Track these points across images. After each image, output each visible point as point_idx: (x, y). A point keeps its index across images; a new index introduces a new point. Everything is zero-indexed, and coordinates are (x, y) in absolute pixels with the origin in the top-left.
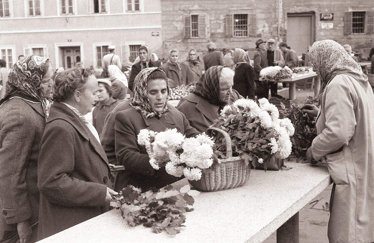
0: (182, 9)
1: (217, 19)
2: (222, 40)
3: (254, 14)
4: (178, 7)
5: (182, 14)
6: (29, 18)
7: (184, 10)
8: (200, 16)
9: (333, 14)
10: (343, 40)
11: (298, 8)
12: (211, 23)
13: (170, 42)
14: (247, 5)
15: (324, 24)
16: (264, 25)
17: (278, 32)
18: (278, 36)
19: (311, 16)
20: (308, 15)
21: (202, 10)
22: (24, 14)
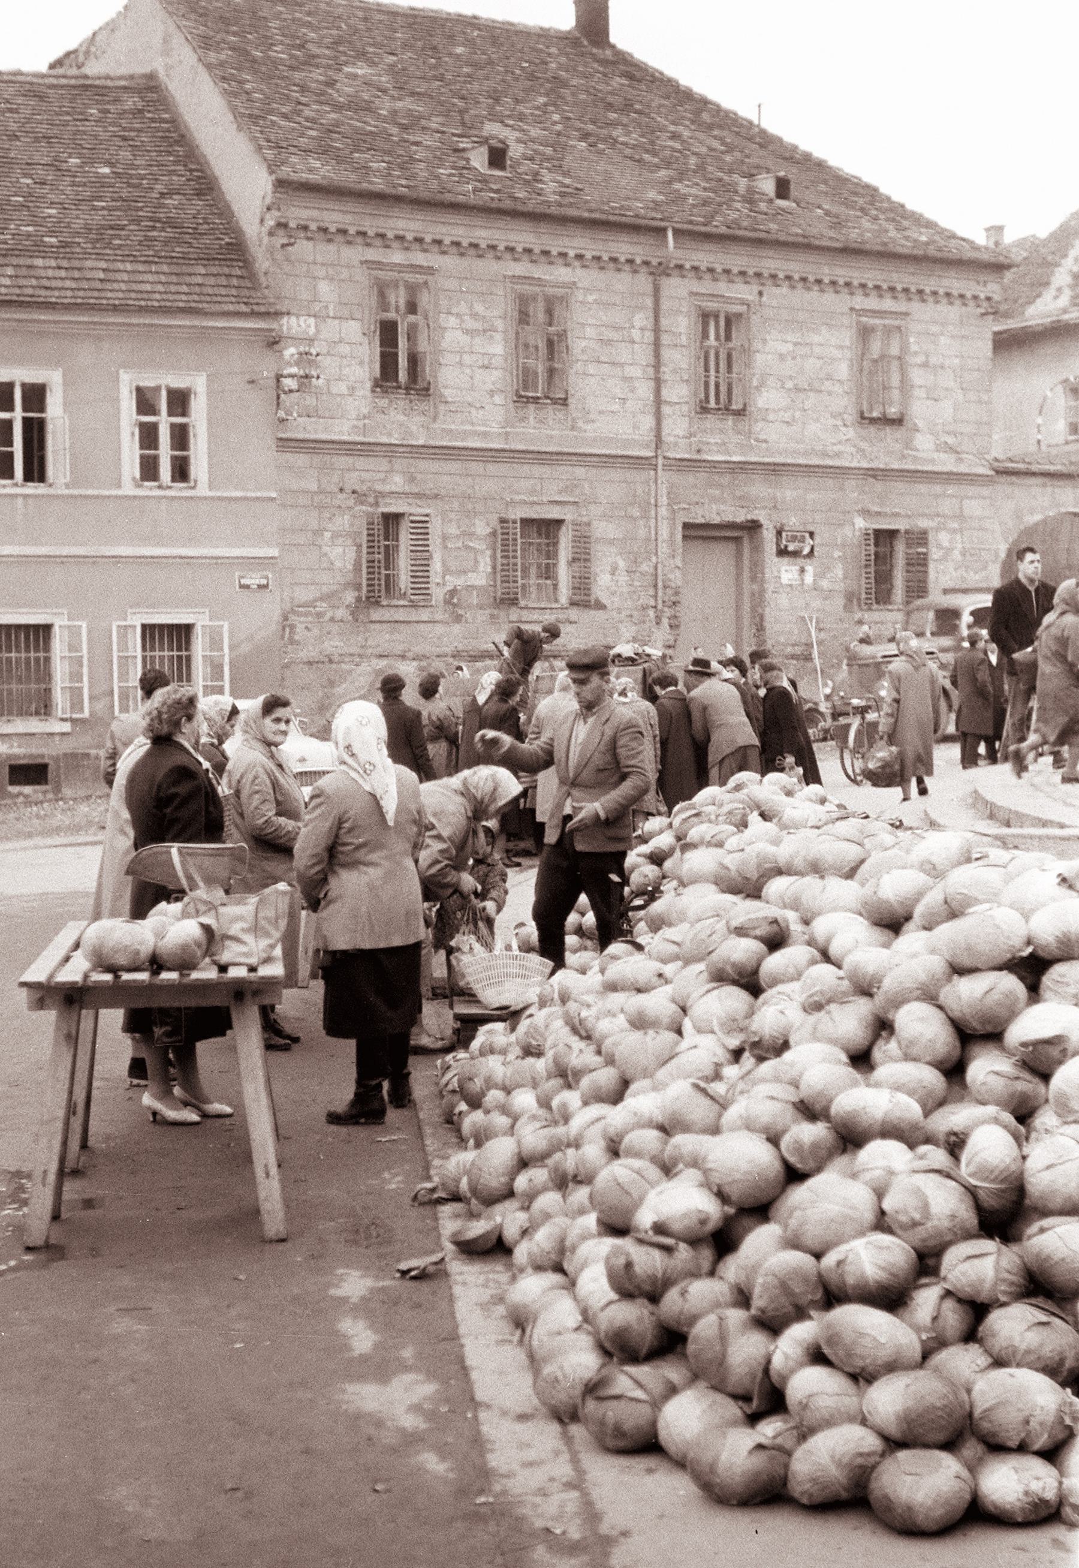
0: (348, 488)
1: (464, 534)
2: (482, 616)
3: (585, 519)
5: (350, 508)
7: (354, 492)
8: (412, 518)
9: (812, 534)
12: (446, 547)
13: (306, 615)
19: (737, 540)
20: (729, 534)
21: (419, 496)
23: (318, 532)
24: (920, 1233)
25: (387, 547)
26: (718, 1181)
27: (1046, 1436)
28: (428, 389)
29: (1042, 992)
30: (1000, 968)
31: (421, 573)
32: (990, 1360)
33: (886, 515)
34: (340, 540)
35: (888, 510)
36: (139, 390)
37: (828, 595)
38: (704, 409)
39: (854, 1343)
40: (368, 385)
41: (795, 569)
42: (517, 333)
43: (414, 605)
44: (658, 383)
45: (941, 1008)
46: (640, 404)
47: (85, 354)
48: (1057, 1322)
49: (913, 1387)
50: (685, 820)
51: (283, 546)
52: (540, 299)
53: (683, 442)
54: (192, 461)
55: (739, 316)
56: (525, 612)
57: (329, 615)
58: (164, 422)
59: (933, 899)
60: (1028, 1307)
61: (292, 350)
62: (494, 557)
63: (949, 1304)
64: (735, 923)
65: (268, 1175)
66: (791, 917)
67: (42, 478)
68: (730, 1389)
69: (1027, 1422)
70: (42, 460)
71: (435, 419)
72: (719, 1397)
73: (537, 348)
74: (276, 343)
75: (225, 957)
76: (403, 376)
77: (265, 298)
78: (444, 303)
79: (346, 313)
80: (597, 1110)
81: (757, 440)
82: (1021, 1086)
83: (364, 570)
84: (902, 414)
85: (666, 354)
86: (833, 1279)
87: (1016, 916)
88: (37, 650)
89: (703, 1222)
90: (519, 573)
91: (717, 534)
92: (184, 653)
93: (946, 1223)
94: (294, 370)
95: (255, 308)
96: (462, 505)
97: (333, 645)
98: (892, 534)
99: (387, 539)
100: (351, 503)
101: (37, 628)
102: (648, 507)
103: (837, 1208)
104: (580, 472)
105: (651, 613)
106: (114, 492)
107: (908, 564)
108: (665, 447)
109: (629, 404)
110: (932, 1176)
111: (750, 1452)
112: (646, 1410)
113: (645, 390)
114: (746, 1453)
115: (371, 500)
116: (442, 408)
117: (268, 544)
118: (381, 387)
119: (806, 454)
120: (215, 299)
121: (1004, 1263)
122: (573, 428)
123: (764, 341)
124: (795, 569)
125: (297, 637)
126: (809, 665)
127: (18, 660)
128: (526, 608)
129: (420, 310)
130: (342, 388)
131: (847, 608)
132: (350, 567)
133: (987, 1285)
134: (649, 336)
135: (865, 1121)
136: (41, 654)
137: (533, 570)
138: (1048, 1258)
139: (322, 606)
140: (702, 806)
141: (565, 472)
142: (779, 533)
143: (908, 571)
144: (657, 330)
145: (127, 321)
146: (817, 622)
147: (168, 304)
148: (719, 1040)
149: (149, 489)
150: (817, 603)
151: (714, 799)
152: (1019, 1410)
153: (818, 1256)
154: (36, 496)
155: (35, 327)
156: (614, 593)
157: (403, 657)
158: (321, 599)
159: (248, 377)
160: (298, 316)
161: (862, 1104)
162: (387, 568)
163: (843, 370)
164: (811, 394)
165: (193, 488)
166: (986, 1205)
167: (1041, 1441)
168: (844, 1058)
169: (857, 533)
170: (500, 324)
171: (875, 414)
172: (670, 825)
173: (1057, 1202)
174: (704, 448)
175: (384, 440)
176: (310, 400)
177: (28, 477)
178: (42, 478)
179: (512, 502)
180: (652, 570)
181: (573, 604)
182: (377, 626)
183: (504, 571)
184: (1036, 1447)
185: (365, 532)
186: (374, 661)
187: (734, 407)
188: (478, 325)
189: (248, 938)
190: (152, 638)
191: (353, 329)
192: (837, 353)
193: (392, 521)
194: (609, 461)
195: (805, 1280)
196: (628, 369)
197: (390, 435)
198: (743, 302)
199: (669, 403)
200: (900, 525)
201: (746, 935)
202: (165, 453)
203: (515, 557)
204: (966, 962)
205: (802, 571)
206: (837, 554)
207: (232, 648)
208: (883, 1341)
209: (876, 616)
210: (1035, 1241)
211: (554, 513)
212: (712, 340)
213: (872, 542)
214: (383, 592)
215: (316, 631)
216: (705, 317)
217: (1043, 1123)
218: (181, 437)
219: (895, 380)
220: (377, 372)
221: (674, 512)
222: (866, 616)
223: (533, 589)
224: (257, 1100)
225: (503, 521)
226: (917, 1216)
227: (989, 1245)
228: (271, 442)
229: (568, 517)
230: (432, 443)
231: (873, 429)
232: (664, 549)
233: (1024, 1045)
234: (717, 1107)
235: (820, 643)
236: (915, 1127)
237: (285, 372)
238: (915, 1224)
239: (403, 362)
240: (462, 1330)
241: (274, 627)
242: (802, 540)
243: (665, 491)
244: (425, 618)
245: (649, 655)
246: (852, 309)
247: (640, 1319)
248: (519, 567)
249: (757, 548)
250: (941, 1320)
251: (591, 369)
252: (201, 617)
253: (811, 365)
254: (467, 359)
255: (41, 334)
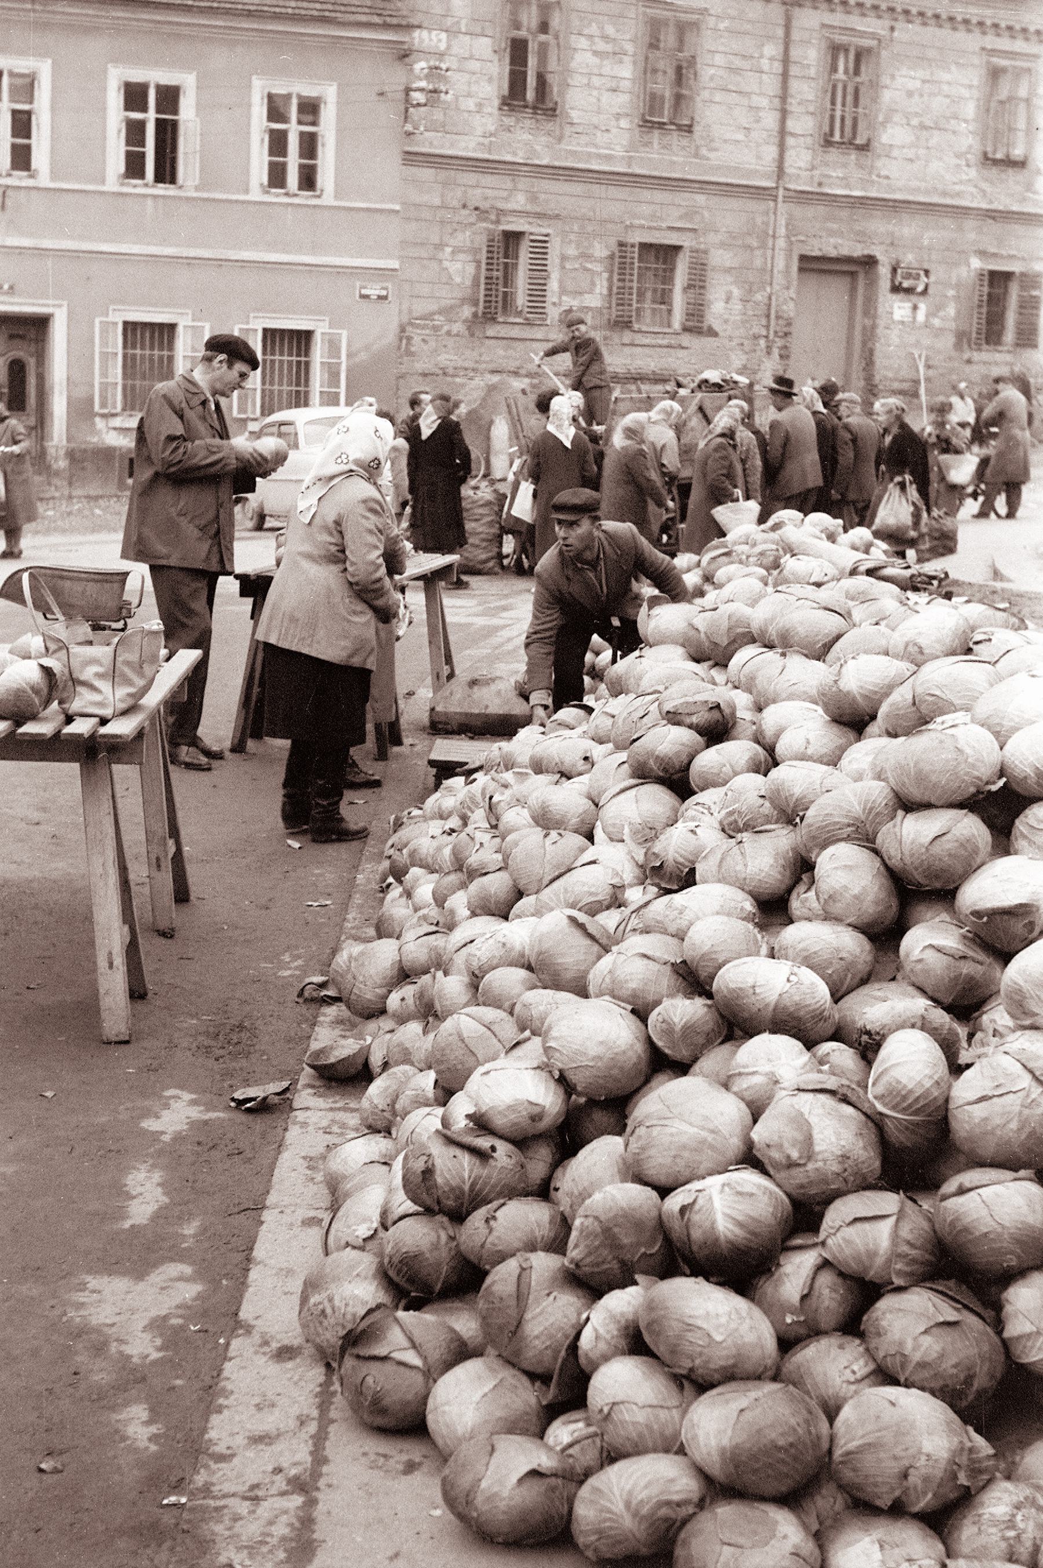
0: (471, 205)
4: (459, 193)
6: (125, 190)
7: (476, 209)
10: (182, 503)
11: (832, 240)
12: (563, 268)
13: (424, 327)
14: (683, 211)
15: (902, 304)
16: (731, 292)
17: (769, 321)
18: (766, 337)
19: (853, 274)
22: (247, 184)
23: (440, 246)
24: (798, 1177)
25: (506, 265)
26: (560, 1065)
27: (930, 1495)
28: (555, 110)
29: (1013, 838)
30: (961, 806)
31: (538, 292)
32: (872, 1366)
33: (1002, 257)
34: (462, 256)
35: (1004, 253)
36: (270, 97)
37: (939, 332)
38: (828, 142)
39: (679, 1337)
40: (496, 102)
41: (908, 305)
42: (647, 58)
43: (529, 323)
44: (784, 113)
45: (876, 852)
46: (765, 134)
47: (220, 58)
48: (972, 1320)
49: (748, 1416)
50: (714, 558)
51: (401, 258)
52: (671, 24)
53: (805, 174)
54: (319, 170)
55: (869, 50)
56: (639, 335)
57: (446, 328)
58: (294, 131)
59: (901, 696)
60: (931, 1294)
61: (423, 64)
62: (610, 280)
63: (826, 1279)
64: (668, 706)
65: (111, 966)
66: (742, 701)
67: (173, 181)
68: (525, 1365)
69: (905, 1476)
70: (174, 161)
71: (560, 139)
72: (508, 1374)
73: (665, 72)
74: (406, 56)
75: (75, 706)
76: (530, 95)
77: (398, 10)
78: (576, 22)
79: (478, 30)
80: (485, 924)
81: (879, 176)
82: (967, 968)
83: (482, 287)
84: (1026, 157)
85: (794, 85)
86: (676, 1226)
87: (987, 738)
88: (161, 349)
89: (535, 1118)
90: (634, 297)
91: (838, 267)
92: (303, 359)
93: (836, 1168)
94: (423, 84)
95: (388, 20)
96: (582, 227)
97: (445, 359)
98: (1007, 276)
99: (506, 256)
100: (472, 219)
101: (161, 326)
102: (766, 237)
103: (693, 1130)
104: (701, 199)
105: (762, 342)
106: (242, 197)
107: (1021, 307)
108: (786, 179)
109: (753, 134)
110: (822, 1097)
111: (521, 1481)
112: (419, 1379)
113: (770, 120)
114: (514, 1479)
115: (493, 217)
116: (568, 130)
117: (389, 256)
118: (508, 105)
119: (927, 192)
120: (349, 9)
121: (906, 1232)
122: (696, 155)
123: (893, 77)
124: (908, 305)
125: (413, 349)
126: (915, 401)
127: (142, 356)
128: (640, 331)
129: (551, 31)
130: (470, 104)
131: (958, 346)
132: (468, 283)
133: (879, 1261)
134: (778, 67)
135: (753, 1003)
136: (165, 353)
137: (649, 295)
138: (966, 1230)
139: (439, 320)
140: (735, 543)
141: (684, 199)
142: (894, 270)
143: (1021, 314)
144: (786, 61)
145: (261, 27)
146: (927, 360)
147: (303, 12)
148: (629, 852)
149: (276, 196)
150: (926, 342)
151: (748, 537)
152: (895, 1458)
153: (664, 1191)
154: (163, 197)
155: (166, 29)
156: (726, 321)
157: (516, 374)
158: (440, 312)
159: (377, 89)
160: (430, 30)
161: (750, 982)
162: (506, 285)
163: (970, 110)
164: (936, 132)
165: (319, 197)
166: (893, 1140)
167: (923, 1502)
168: (749, 906)
169: (972, 274)
170: (629, 48)
171: (999, 156)
172: (698, 564)
173: (988, 1149)
174: (824, 180)
175: (509, 158)
176: (438, 115)
177: (159, 178)
178: (173, 181)
179: (632, 226)
180: (766, 301)
181: (686, 329)
182: (493, 341)
183: (619, 295)
184: (916, 1509)
185: (485, 249)
186: (488, 376)
187: (858, 141)
188: (609, 48)
189: (104, 686)
190: (273, 342)
191: (484, 46)
192: (965, 93)
193: (512, 238)
194: (729, 190)
195: (638, 1225)
196: (754, 97)
197: (515, 154)
198: (873, 36)
199: (792, 134)
200: (1015, 267)
201: (678, 723)
202: (293, 161)
203: (632, 281)
204: (916, 793)
205: (915, 308)
206: (951, 293)
207: (349, 356)
208: (719, 1338)
209: (984, 356)
210: (952, 1203)
211: (672, 239)
212: (840, 75)
213: (986, 283)
214: (500, 309)
215: (432, 344)
216: (836, 50)
217: (993, 1021)
218: (309, 145)
219: (1021, 124)
220: (506, 92)
221: (791, 243)
222: (976, 356)
223: (648, 313)
224: (104, 875)
225: (621, 244)
226: (795, 1155)
227: (889, 1202)
228: (398, 159)
229: (686, 244)
230: (557, 164)
231: (995, 170)
232: (779, 279)
233: (977, 914)
234: (596, 948)
235: (928, 380)
236: (819, 1016)
237: (414, 86)
238: (791, 1165)
239: (531, 81)
240: (271, 1199)
241: (391, 337)
242: (917, 277)
243: (783, 222)
244: (539, 336)
245: (735, 382)
246: (983, 49)
247: (435, 1246)
248: (635, 291)
249: (872, 283)
250: (813, 1301)
251: (718, 97)
252: (321, 324)
253: (938, 104)
254: (596, 81)
255: (179, 36)
